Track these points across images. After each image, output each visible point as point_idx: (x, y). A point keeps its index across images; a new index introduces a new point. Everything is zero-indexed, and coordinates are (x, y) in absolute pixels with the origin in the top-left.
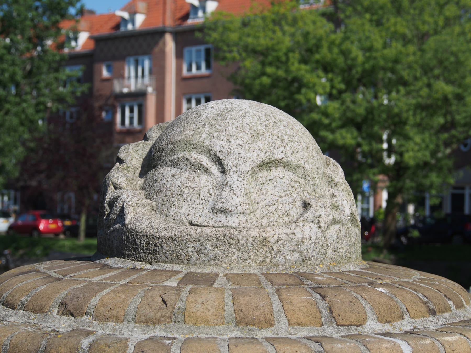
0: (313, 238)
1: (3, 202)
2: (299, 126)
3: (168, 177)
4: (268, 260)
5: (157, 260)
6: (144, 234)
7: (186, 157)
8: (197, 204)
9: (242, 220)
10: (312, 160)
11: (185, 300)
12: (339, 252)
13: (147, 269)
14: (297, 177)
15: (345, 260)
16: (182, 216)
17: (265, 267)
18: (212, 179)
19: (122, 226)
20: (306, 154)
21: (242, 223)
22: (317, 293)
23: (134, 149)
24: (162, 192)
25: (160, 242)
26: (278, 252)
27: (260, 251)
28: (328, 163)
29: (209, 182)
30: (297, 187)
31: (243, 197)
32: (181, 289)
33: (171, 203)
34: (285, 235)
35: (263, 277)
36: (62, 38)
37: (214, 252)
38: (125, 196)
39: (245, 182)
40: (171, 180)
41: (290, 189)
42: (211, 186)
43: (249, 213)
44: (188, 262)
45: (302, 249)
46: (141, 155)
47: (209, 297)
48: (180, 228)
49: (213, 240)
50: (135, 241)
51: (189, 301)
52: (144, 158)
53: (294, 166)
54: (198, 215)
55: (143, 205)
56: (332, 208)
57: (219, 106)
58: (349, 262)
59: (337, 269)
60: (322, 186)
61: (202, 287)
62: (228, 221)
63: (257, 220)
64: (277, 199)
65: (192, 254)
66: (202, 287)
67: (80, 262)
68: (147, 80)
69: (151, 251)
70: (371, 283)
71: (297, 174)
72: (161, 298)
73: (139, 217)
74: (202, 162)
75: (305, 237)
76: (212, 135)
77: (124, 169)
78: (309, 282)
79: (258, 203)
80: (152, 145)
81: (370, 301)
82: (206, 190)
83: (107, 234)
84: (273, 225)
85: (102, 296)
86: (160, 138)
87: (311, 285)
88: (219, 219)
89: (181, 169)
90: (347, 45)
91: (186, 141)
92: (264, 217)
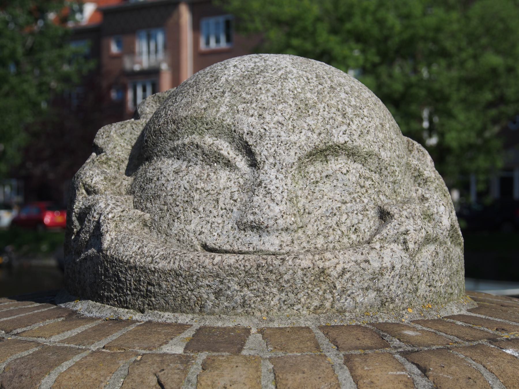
0: (398, 266)
1: (4, 192)
2: (367, 93)
3: (169, 174)
4: (328, 305)
5: (152, 307)
6: (131, 265)
7: (195, 142)
8: (215, 217)
9: (285, 240)
10: (389, 145)
11: (195, 381)
12: (435, 287)
13: (137, 321)
14: (368, 171)
15: (444, 298)
16: (191, 235)
17: (324, 315)
19: (98, 252)
20: (381, 135)
21: (285, 245)
22: (413, 363)
23: (118, 131)
24: (160, 198)
25: (156, 278)
26: (343, 291)
27: (315, 290)
28: (410, 148)
29: (232, 182)
30: (368, 186)
31: (286, 204)
32: (189, 361)
33: (174, 214)
34: (353, 263)
35: (321, 334)
36: (65, 12)
37: (242, 294)
38: (102, 205)
39: (289, 181)
40: (174, 178)
41: (359, 190)
42: (235, 188)
43: (296, 229)
44: (201, 310)
45: (380, 285)
46: (129, 141)
47: (235, 377)
48: (188, 255)
49: (240, 274)
50: (118, 276)
51: (203, 383)
52: (133, 145)
53: (363, 154)
54: (216, 234)
55: (130, 219)
56: (425, 218)
57: (246, 64)
58: (450, 301)
59: (434, 315)
60: (406, 184)
61: (223, 356)
62: (264, 243)
63: (308, 239)
64: (338, 206)
65: (206, 297)
66: (223, 356)
67: (37, 305)
68: (161, 56)
69: (143, 292)
70: (493, 340)
71: (368, 167)
72: (155, 378)
73: (124, 238)
74: (221, 149)
75: (384, 265)
76: (235, 107)
77: (102, 163)
78: (396, 342)
79: (309, 213)
80: (144, 125)
81: (500, 375)
82: (227, 193)
83: (76, 263)
84: (334, 248)
85: (61, 374)
86: (157, 115)
87: (400, 347)
88: (248, 239)
89: (189, 162)
90: (381, 14)
91: (196, 119)
92: (318, 234)
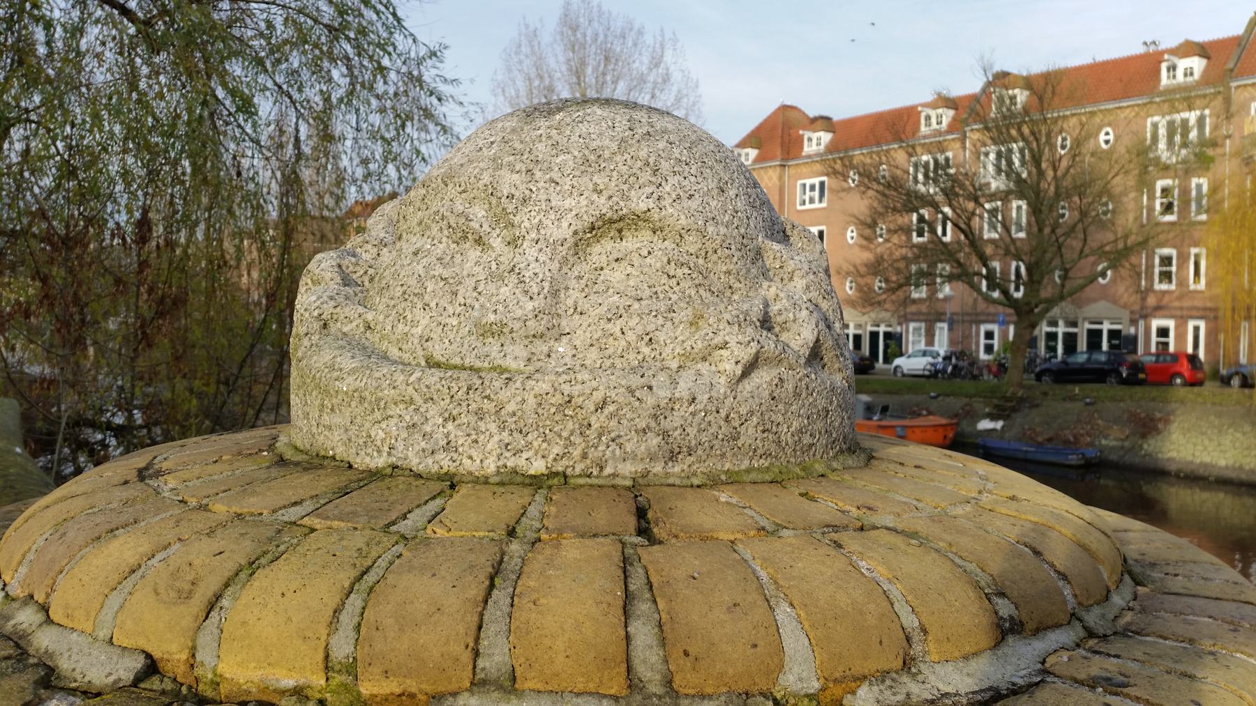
0: (703, 398)
4: (577, 453)
18: (489, 259)
62: (505, 356)
64: (628, 303)
82: (470, 283)
